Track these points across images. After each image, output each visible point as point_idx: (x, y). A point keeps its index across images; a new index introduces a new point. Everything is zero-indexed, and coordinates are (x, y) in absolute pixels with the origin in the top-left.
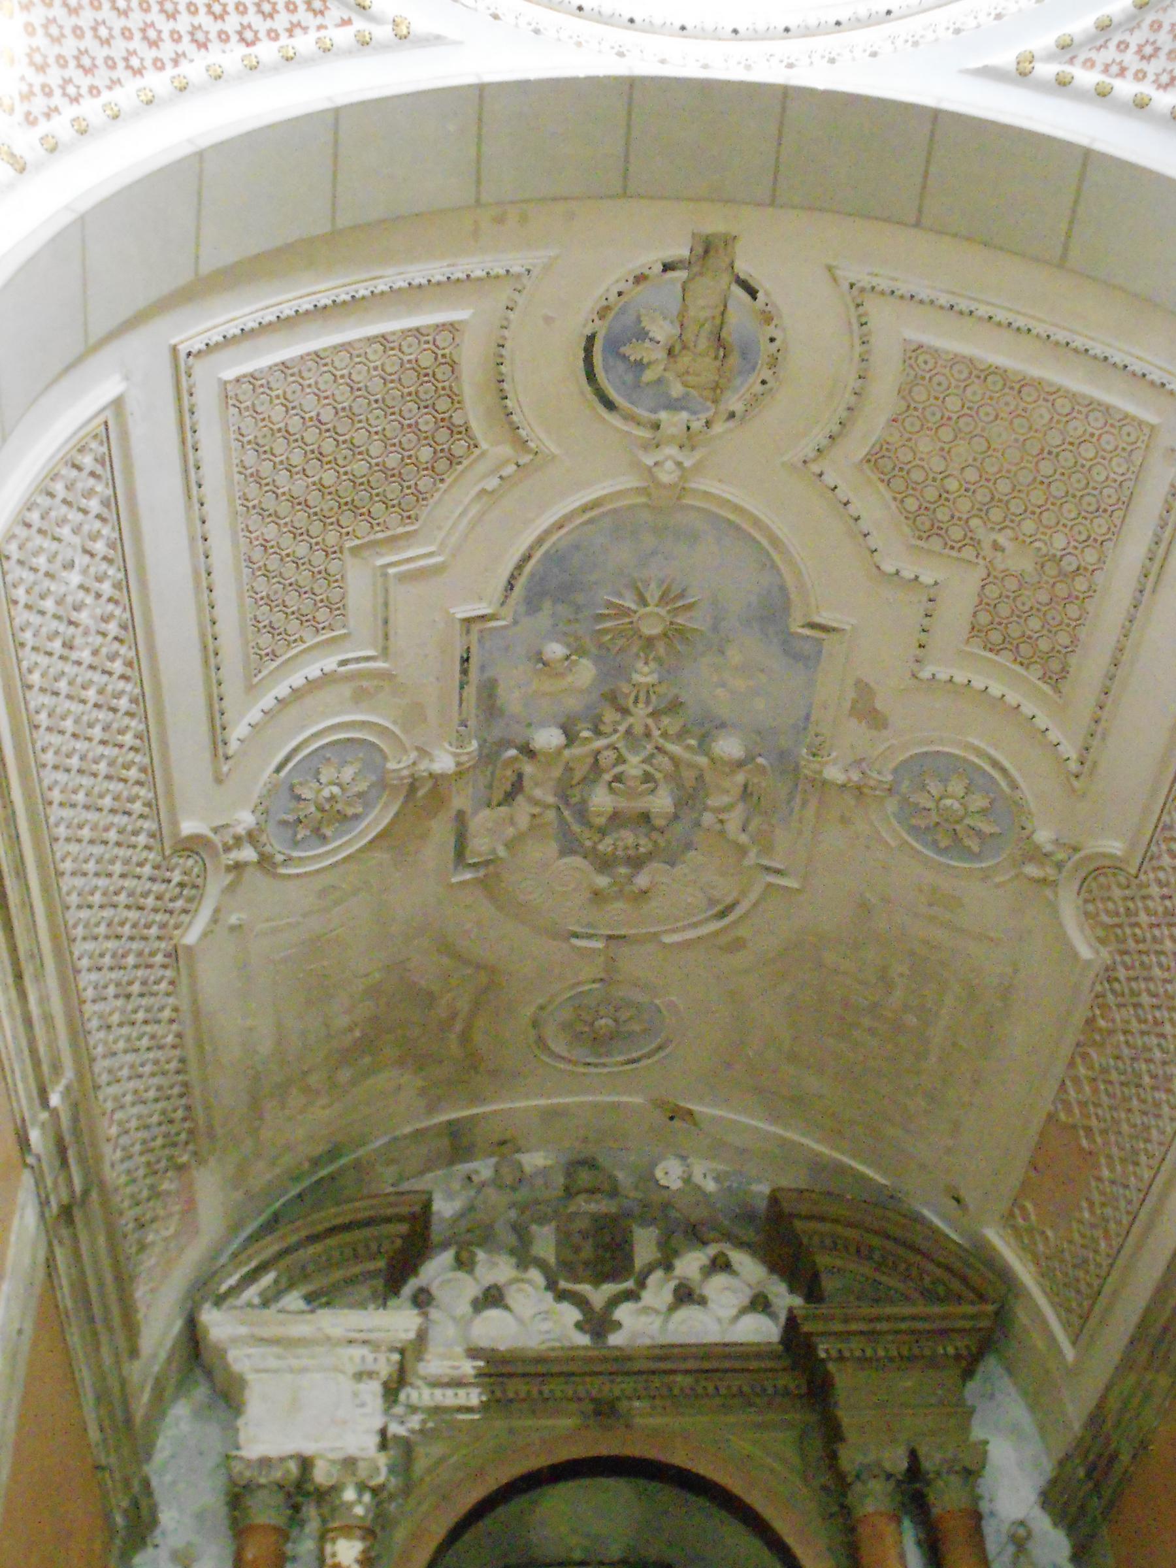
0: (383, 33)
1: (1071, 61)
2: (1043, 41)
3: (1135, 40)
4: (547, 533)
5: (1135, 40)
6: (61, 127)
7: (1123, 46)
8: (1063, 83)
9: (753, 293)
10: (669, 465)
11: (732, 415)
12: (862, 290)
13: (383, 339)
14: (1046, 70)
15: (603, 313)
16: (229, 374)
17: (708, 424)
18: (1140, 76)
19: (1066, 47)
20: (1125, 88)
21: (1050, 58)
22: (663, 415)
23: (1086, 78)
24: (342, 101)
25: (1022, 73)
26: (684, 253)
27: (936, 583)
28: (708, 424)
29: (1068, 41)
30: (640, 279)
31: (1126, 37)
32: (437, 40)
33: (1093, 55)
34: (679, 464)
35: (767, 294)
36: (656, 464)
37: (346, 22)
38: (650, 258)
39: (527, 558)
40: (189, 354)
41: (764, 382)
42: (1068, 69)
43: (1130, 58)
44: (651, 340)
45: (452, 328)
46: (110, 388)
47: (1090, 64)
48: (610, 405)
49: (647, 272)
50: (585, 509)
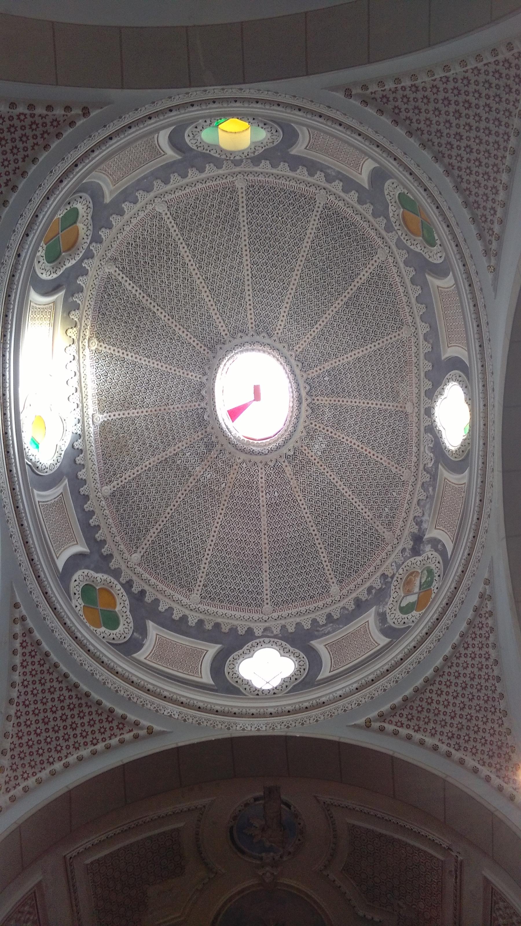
0: (143, 733)
1: (384, 721)
2: (374, 714)
3: (405, 713)
4: (225, 903)
5: (405, 713)
6: (18, 791)
7: (401, 715)
8: (382, 730)
9: (289, 806)
10: (268, 874)
11: (290, 853)
12: (328, 804)
13: (150, 838)
14: (376, 725)
15: (235, 818)
16: (88, 861)
17: (281, 857)
18: (408, 726)
19: (381, 715)
20: (403, 731)
21: (376, 721)
22: (263, 854)
23: (390, 728)
24: (125, 761)
25: (368, 725)
26: (262, 794)
27: (380, 921)
28: (281, 857)
29: (382, 714)
30: (246, 805)
31: (402, 712)
32: (163, 733)
33: (392, 718)
34: (273, 874)
35: (295, 807)
36: (263, 874)
37: (131, 731)
38: (249, 797)
39: (218, 914)
40: (71, 858)
41: (299, 840)
42: (383, 724)
43: (404, 720)
44: (254, 826)
45: (178, 830)
46: (37, 878)
47: (391, 722)
48: (243, 852)
49: (249, 802)
50: (239, 893)
